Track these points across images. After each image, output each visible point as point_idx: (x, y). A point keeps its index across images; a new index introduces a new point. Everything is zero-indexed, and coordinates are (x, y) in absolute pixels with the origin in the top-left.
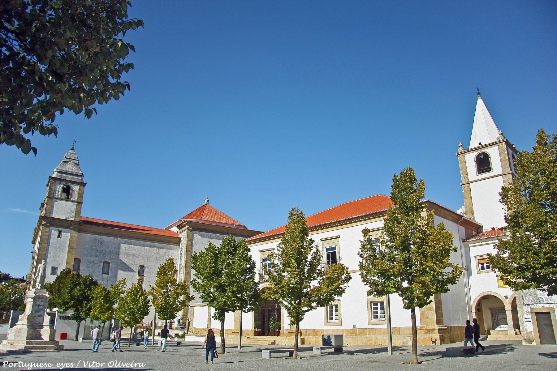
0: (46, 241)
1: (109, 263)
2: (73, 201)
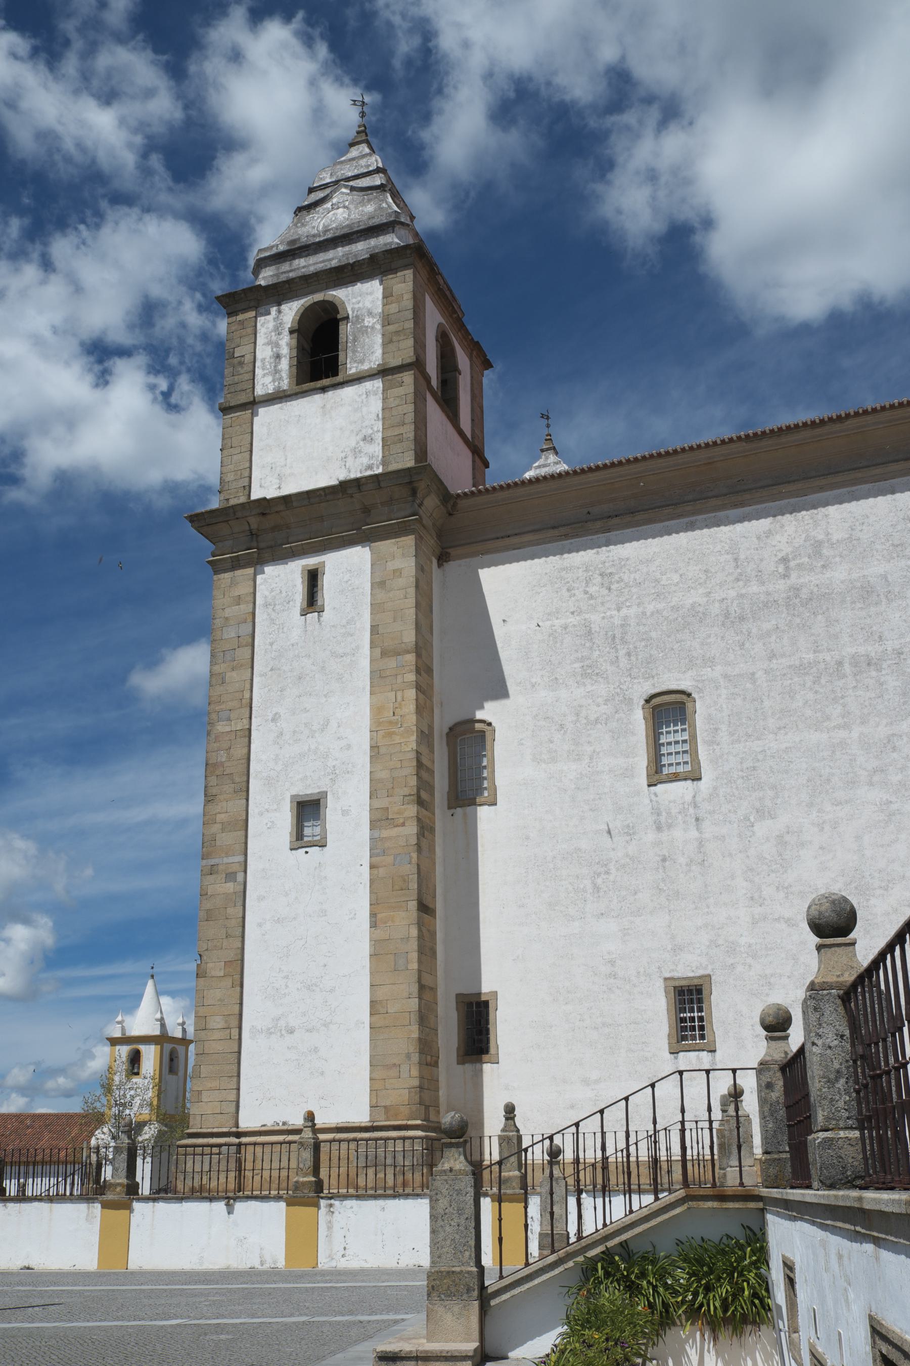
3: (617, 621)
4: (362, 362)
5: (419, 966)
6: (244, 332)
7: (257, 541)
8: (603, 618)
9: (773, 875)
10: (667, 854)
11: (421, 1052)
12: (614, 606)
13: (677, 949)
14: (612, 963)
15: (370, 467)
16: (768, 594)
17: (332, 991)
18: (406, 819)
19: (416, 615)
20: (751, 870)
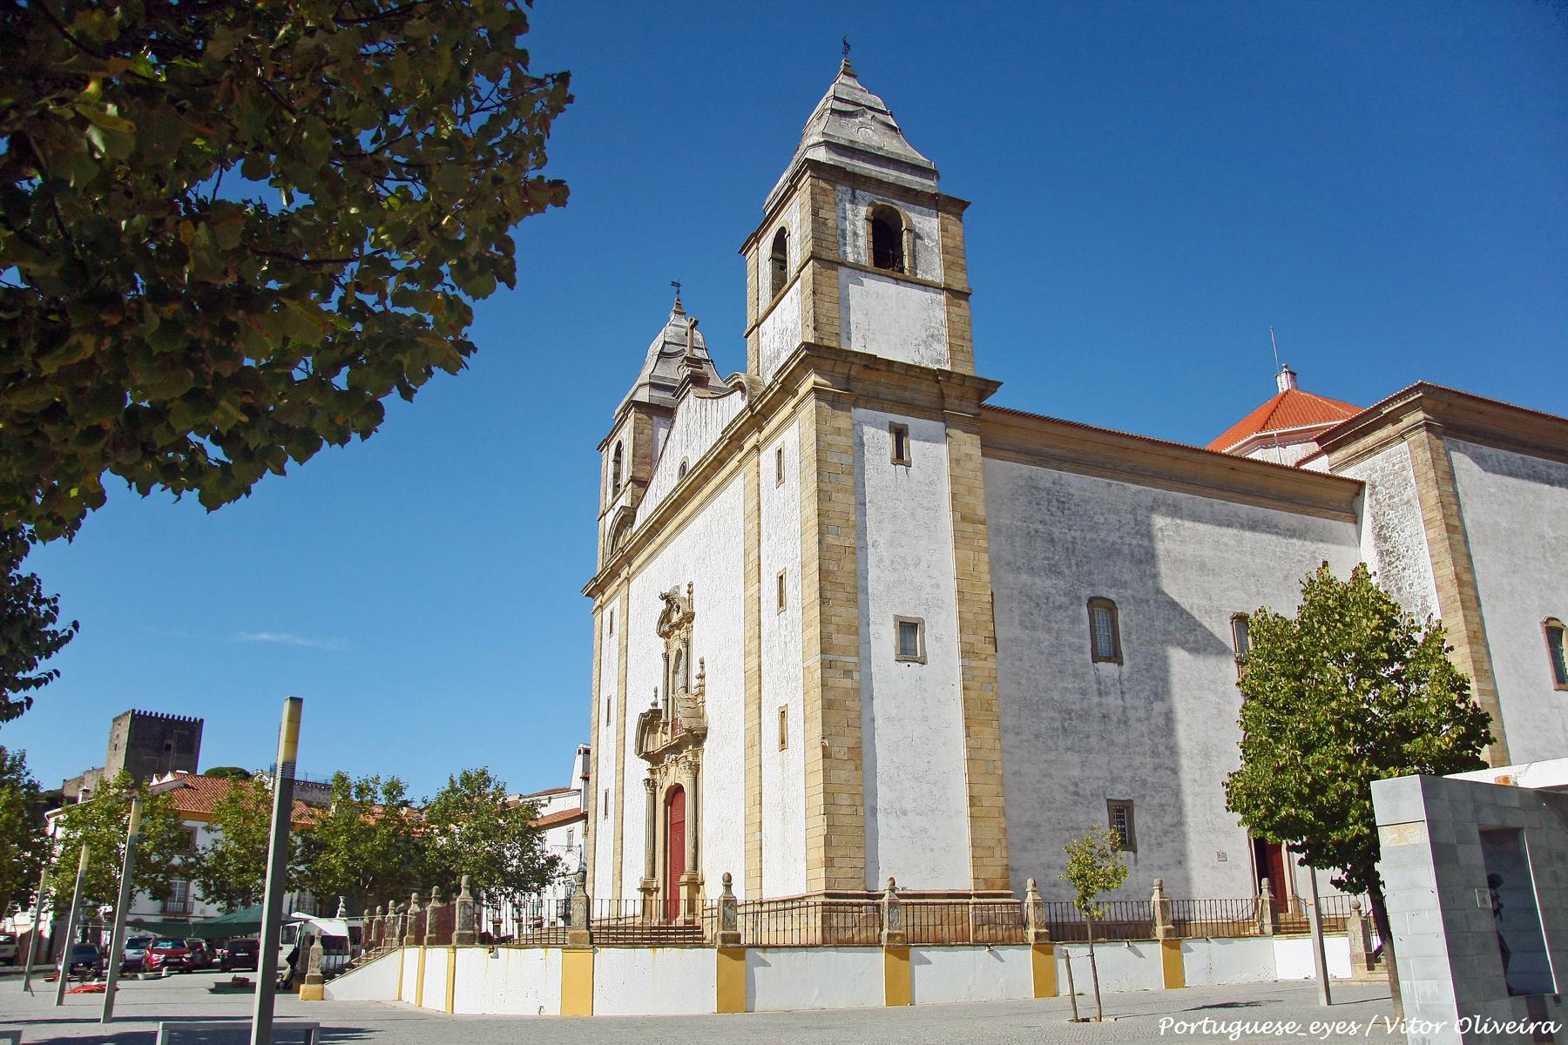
0: (849, 481)
2: (925, 285)
13: (1114, 780)
17: (936, 783)
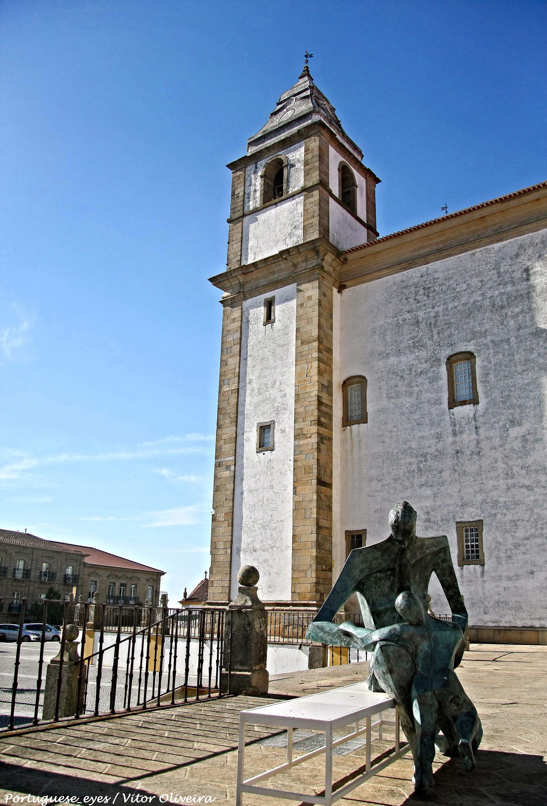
1: (469, 356)
3: (432, 314)
4: (294, 187)
5: (317, 516)
6: (239, 181)
7: (243, 289)
8: (425, 313)
9: (520, 460)
10: (459, 449)
11: (318, 563)
12: (431, 306)
13: (464, 505)
14: (428, 513)
15: (298, 242)
16: (517, 291)
17: (275, 529)
18: (312, 434)
19: (319, 320)
20: (507, 457)
